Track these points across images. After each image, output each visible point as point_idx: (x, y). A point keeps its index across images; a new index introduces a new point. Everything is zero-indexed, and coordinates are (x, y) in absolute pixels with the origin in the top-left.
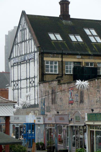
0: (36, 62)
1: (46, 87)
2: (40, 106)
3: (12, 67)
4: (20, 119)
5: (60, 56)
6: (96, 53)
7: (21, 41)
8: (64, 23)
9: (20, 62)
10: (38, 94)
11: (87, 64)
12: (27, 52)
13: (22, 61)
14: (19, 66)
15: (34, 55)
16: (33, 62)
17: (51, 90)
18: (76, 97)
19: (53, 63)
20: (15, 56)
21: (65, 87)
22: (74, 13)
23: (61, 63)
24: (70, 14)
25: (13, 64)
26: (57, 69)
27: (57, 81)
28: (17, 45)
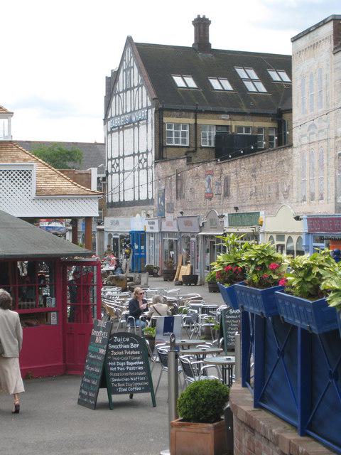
0: (150, 125)
1: (167, 169)
2: (157, 203)
5: (192, 114)
6: (253, 111)
8: (202, 56)
9: (123, 126)
11: (240, 129)
13: (126, 124)
15: (147, 112)
19: (179, 126)
23: (193, 127)
24: (211, 41)
26: (187, 138)
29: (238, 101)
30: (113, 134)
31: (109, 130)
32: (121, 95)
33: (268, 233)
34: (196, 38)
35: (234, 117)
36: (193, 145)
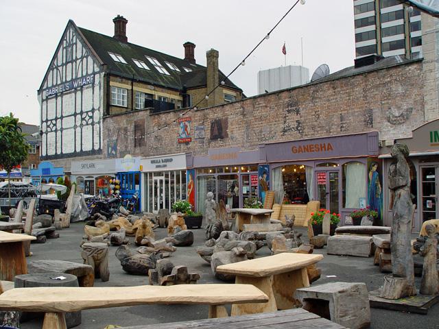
0: (97, 88)
2: (106, 152)
3: (45, 102)
4: (97, 167)
5: (130, 82)
7: (64, 62)
9: (62, 93)
10: (102, 134)
12: (76, 76)
13: (66, 91)
14: (59, 98)
15: (94, 78)
16: (91, 89)
17: (133, 126)
18: (197, 132)
20: (50, 85)
23: (130, 92)
25: (47, 97)
26: (126, 100)
27: (149, 111)
28: (55, 70)
30: (49, 101)
31: (44, 98)
32: (60, 68)
34: (115, 32)
35: (157, 89)
36: (130, 107)
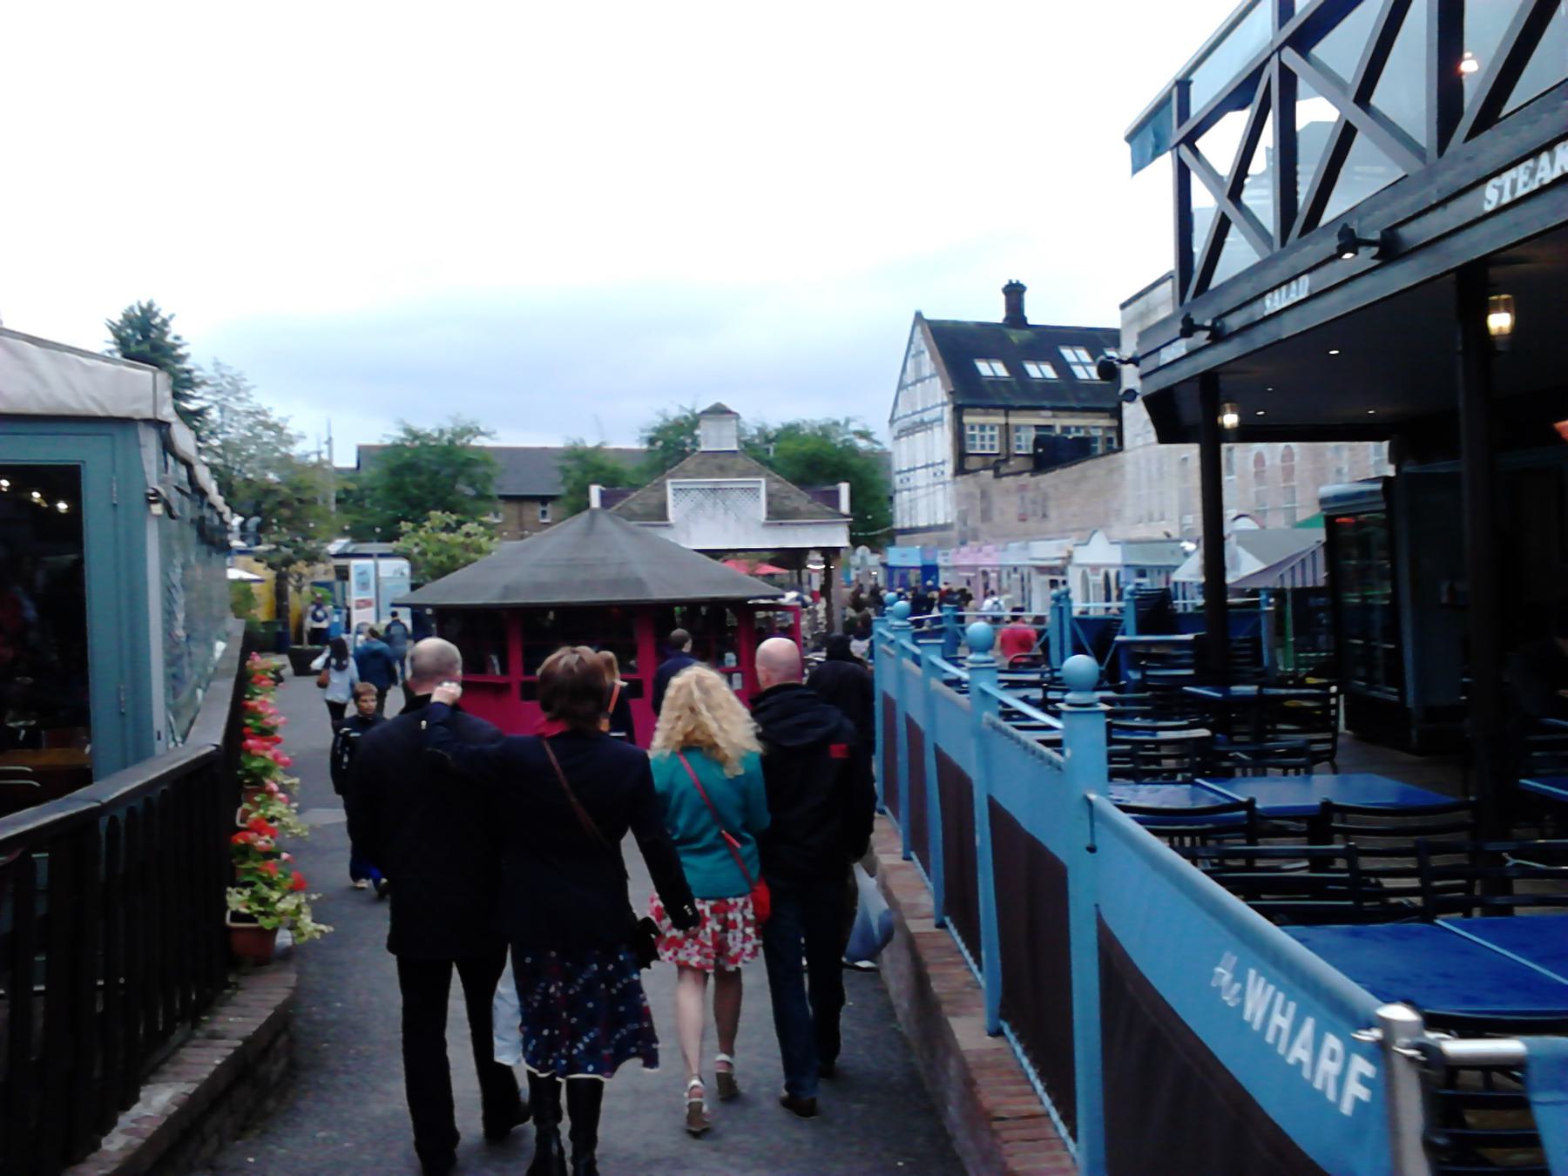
8: (1016, 335)
11: (1066, 429)
19: (986, 428)
21: (1008, 481)
22: (1036, 313)
29: (1065, 394)
33: (1080, 565)
